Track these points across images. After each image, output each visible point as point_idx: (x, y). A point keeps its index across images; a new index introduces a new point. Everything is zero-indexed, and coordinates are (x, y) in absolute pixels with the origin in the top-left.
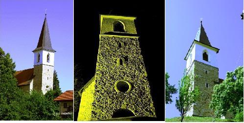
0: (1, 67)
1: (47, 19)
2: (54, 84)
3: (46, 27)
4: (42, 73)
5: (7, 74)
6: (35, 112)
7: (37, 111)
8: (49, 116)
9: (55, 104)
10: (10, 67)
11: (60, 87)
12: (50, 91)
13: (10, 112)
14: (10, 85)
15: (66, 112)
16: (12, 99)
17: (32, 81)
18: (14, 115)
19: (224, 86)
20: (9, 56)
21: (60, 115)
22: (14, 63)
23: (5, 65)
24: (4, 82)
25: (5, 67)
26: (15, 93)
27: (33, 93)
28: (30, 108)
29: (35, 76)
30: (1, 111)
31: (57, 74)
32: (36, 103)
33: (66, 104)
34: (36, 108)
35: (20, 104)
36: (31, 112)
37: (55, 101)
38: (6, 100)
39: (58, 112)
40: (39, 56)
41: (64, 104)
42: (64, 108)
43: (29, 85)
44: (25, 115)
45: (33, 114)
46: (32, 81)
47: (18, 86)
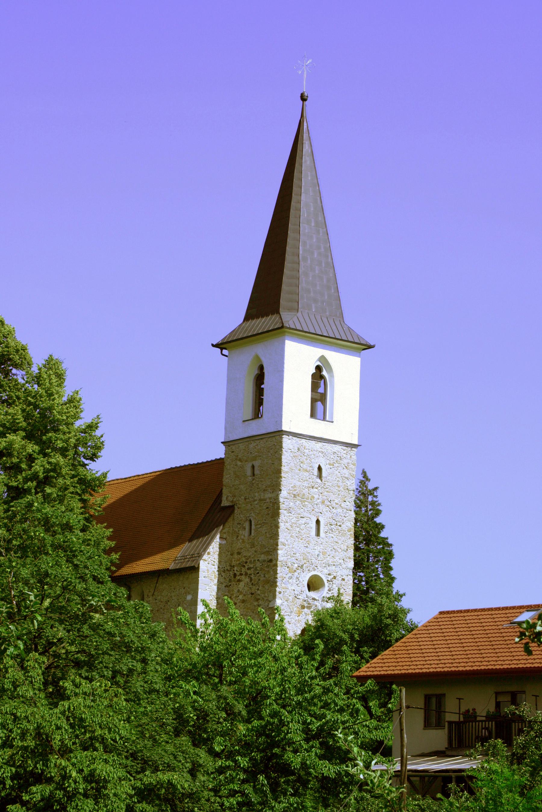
0: (6, 452)
1: (310, 124)
2: (358, 565)
3: (306, 161)
4: (276, 487)
5: (47, 498)
6: (230, 755)
7: (247, 747)
8: (324, 780)
9: (364, 699)
10: (63, 451)
11: (397, 587)
12: (336, 613)
13: (65, 752)
14: (66, 570)
15: (441, 754)
16: (78, 664)
17: (214, 548)
18: (91, 778)
19: (175, 737)
20: (60, 376)
21: (398, 775)
22: (92, 427)
23: (29, 437)
24: (23, 550)
25: (32, 448)
26: (95, 628)
27: (221, 628)
28: (200, 728)
29: (231, 509)
30: (7, 743)
31: (381, 497)
32: (239, 694)
33: (440, 698)
34: (242, 728)
35: (135, 699)
36: (203, 756)
37: (362, 679)
38: (37, 674)
39: (387, 753)
40: (260, 378)
41: (427, 698)
42: (427, 725)
43: (195, 569)
44: (164, 777)
45: (221, 771)
46: (214, 548)
47: (119, 580)
